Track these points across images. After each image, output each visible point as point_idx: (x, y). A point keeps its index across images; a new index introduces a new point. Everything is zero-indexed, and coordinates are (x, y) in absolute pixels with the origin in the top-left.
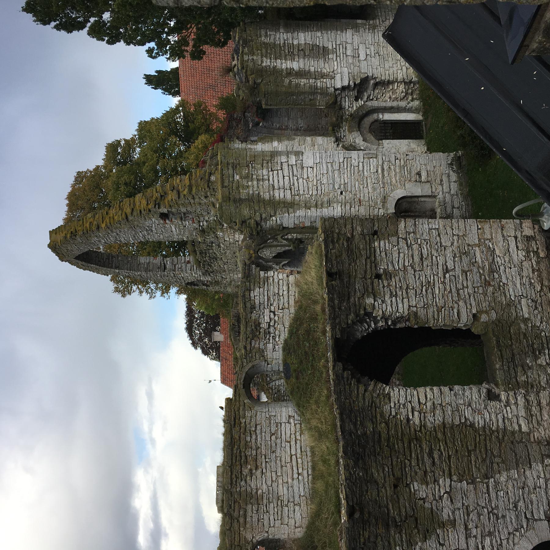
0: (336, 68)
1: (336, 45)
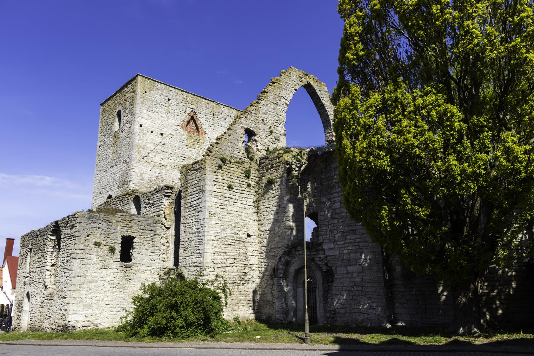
0: (339, 243)
1: (359, 242)
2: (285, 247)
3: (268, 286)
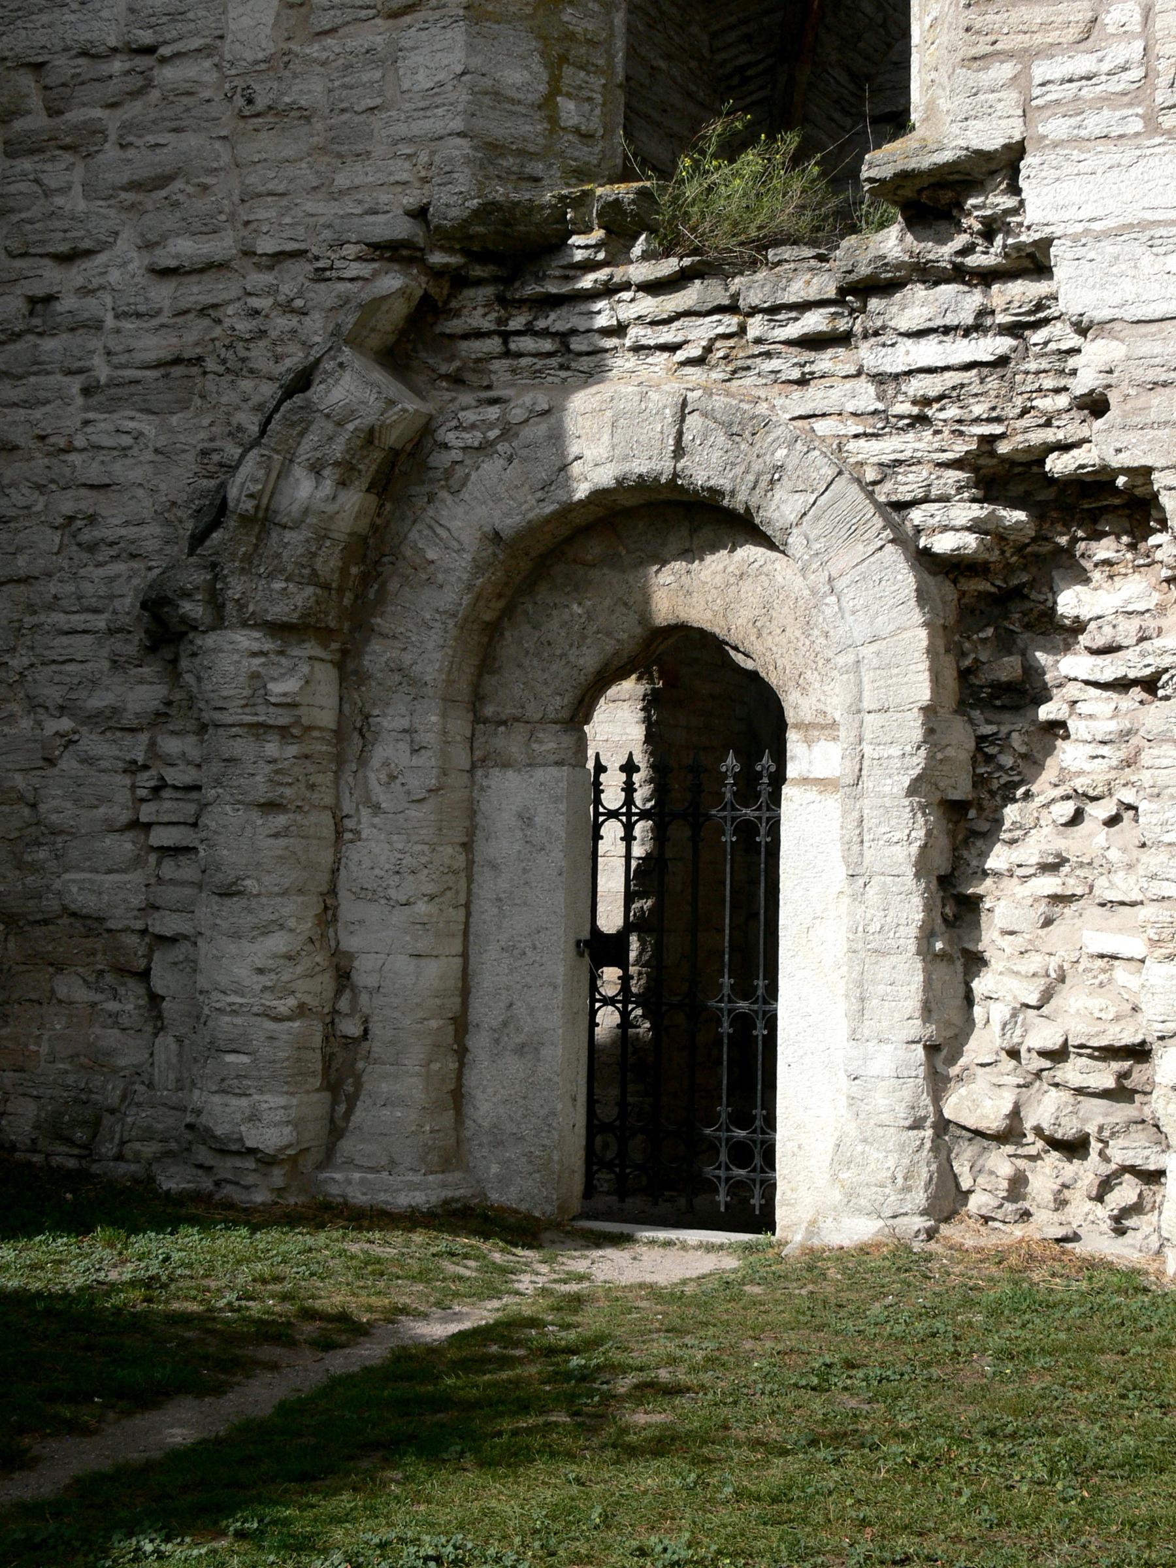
2: (389, 252)
3: (94, 743)
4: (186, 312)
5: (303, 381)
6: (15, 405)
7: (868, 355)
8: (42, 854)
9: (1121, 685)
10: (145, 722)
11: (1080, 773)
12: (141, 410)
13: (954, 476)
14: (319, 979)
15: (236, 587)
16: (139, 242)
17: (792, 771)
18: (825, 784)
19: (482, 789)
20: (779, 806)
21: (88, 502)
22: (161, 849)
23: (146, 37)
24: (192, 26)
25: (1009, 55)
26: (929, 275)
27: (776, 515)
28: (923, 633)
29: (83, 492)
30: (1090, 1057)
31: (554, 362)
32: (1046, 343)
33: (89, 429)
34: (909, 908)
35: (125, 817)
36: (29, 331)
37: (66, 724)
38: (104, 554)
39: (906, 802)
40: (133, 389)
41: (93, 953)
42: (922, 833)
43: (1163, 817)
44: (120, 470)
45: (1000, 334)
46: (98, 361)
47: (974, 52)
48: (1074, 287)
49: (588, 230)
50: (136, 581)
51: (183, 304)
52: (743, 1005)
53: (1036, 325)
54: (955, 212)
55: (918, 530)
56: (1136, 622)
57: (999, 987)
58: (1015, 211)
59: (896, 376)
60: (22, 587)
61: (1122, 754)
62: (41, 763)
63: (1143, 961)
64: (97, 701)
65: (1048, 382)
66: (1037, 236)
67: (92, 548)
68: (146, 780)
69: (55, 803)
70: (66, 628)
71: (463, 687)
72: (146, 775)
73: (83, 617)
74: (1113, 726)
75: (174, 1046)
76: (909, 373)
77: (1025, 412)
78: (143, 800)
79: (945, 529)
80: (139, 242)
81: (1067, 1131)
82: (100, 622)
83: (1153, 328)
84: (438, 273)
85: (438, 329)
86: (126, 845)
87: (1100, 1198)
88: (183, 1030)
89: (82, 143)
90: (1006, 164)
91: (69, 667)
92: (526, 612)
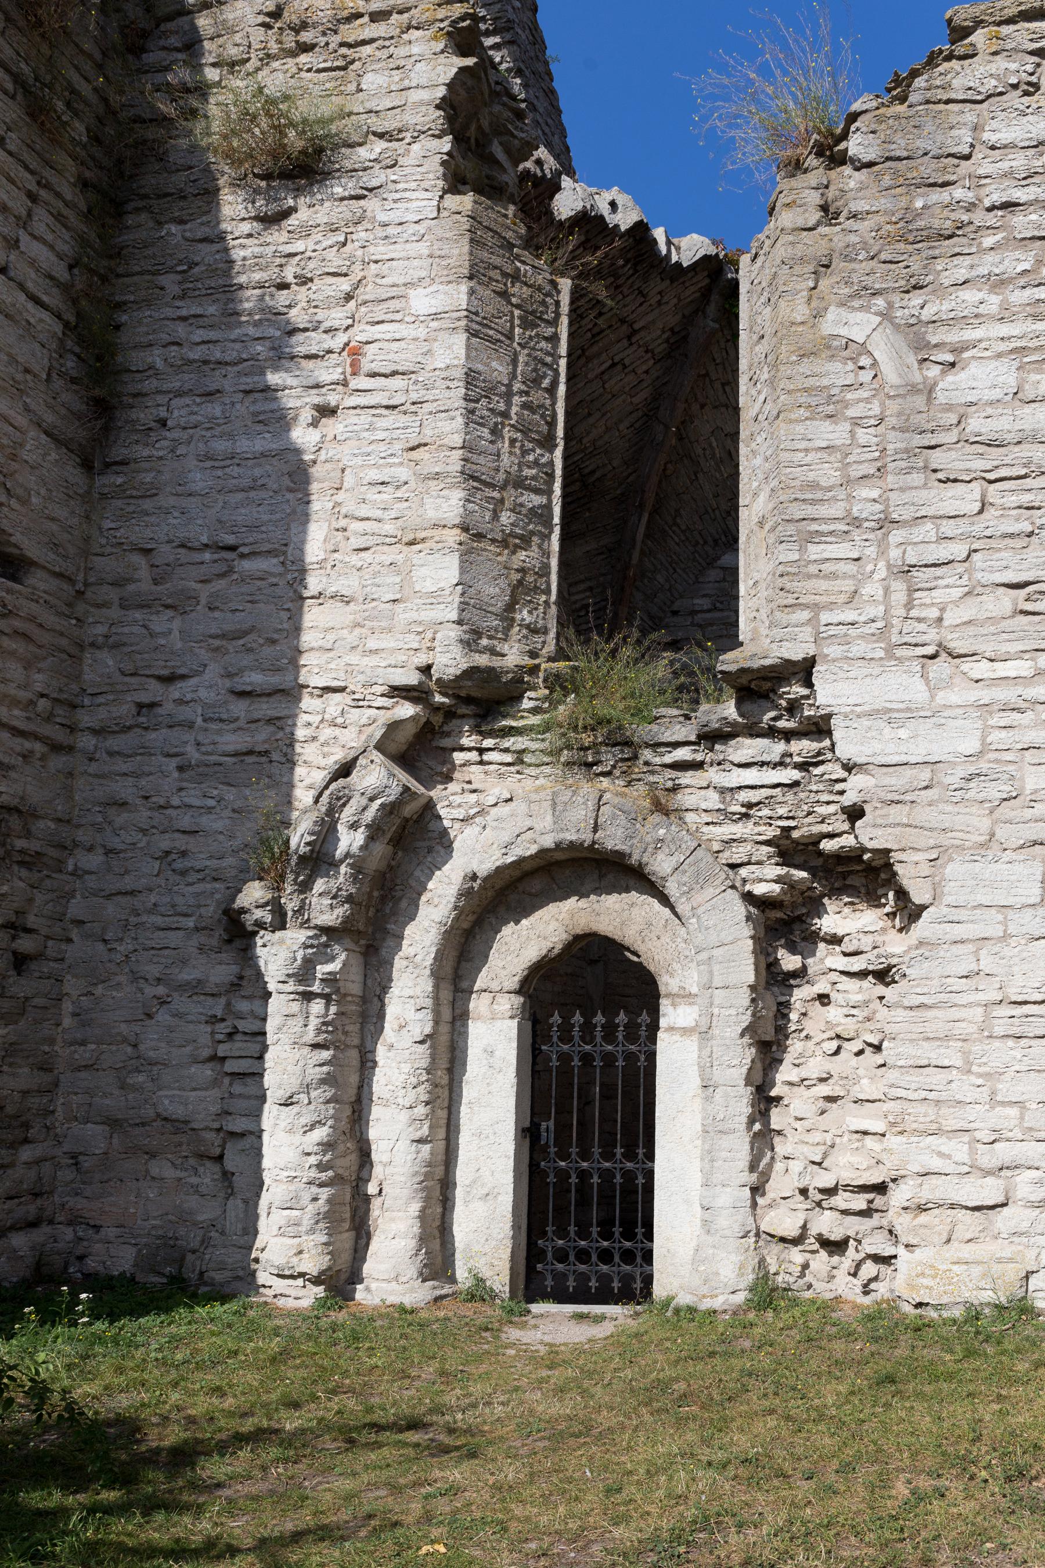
2: (399, 692)
3: (180, 1002)
4: (258, 720)
5: (345, 770)
6: (125, 774)
7: (713, 775)
8: (141, 1078)
9: (862, 974)
10: (223, 990)
11: (838, 1025)
12: (223, 783)
13: (766, 849)
14: (349, 1158)
15: (290, 905)
16: (222, 672)
17: (663, 1022)
18: (686, 1031)
19: (460, 1034)
20: (655, 1044)
21: (181, 842)
22: (232, 1074)
23: (230, 540)
24: (264, 536)
25: (806, 606)
26: (753, 731)
27: (658, 869)
28: (750, 942)
29: (176, 835)
30: (852, 1192)
31: (512, 769)
32: (822, 775)
33: (183, 794)
34: (739, 1103)
35: (206, 1053)
36: (137, 726)
37: (161, 990)
38: (193, 877)
39: (739, 1042)
40: (217, 768)
41: (180, 1144)
42: (749, 1061)
43: (897, 1051)
44: (205, 821)
45: (795, 768)
46: (190, 749)
47: (786, 602)
48: (847, 742)
49: (534, 688)
50: (217, 896)
51: (256, 715)
52: (629, 1165)
53: (816, 764)
54: (771, 695)
55: (744, 881)
56: (870, 937)
57: (794, 1148)
58: (807, 697)
59: (732, 789)
60: (129, 898)
61: (865, 1014)
62: (142, 1017)
63: (884, 1135)
64: (186, 975)
65: (825, 797)
66: (823, 712)
67: (183, 873)
68: (223, 1028)
69: (153, 1043)
70: (163, 926)
71: (448, 969)
72: (223, 1025)
73: (176, 919)
74: (859, 997)
75: (241, 1205)
76: (740, 788)
77: (809, 814)
78: (220, 1042)
79: (761, 880)
80: (222, 672)
81: (835, 1236)
82: (190, 923)
83: (891, 769)
84: (437, 708)
85: (434, 744)
86: (208, 1072)
87: (855, 1275)
88: (248, 1195)
89: (179, 605)
90: (804, 670)
91: (166, 952)
92: (491, 924)
